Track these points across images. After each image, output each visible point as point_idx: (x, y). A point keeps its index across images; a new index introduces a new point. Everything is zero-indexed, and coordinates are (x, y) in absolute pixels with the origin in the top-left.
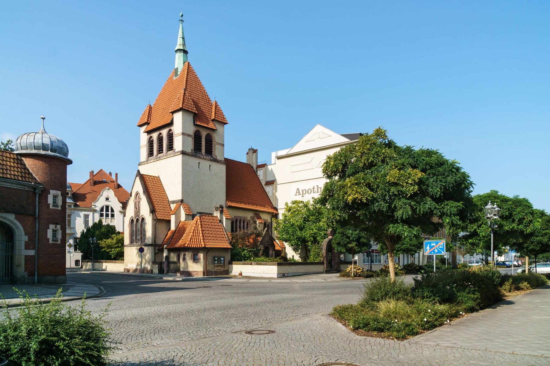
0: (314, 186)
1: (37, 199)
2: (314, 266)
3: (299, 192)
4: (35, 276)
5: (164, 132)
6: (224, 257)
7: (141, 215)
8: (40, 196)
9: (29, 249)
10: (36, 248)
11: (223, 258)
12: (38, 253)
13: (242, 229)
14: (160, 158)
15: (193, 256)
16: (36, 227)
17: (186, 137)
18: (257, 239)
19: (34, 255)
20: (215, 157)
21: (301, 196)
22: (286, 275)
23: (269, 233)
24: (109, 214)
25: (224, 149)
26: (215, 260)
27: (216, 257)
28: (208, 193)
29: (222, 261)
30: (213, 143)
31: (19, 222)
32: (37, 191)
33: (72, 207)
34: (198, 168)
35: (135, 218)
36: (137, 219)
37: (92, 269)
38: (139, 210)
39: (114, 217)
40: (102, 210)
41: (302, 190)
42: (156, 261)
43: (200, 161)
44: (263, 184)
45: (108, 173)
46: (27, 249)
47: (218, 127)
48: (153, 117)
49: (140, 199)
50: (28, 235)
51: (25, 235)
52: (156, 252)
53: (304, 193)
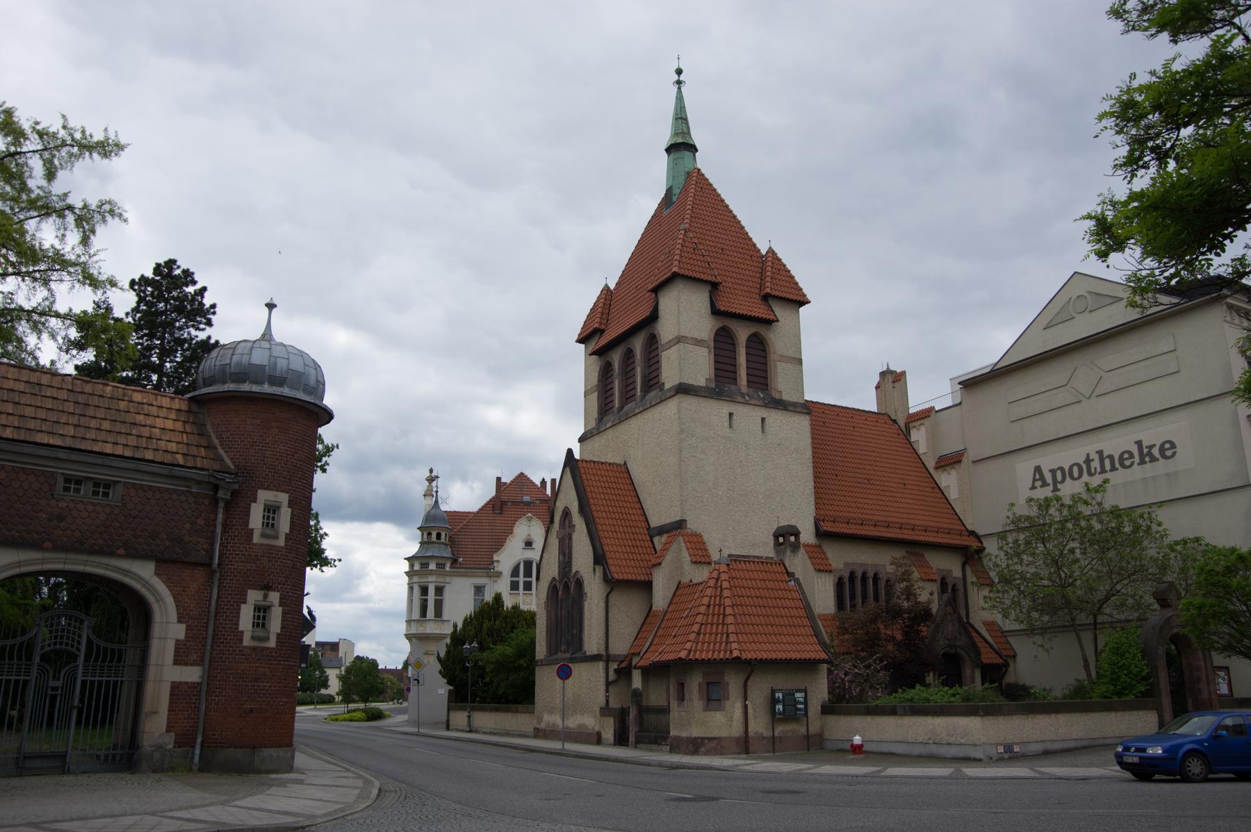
0: (1088, 455)
1: (220, 516)
2: (1119, 714)
3: (1042, 478)
4: (193, 747)
5: (638, 344)
6: (805, 691)
7: (574, 570)
8: (229, 505)
9: (186, 664)
10: (207, 662)
12: (209, 676)
13: (871, 599)
16: (211, 597)
17: (690, 346)
18: (917, 631)
19: (199, 680)
20: (777, 396)
21: (1051, 488)
22: (1016, 749)
23: (955, 611)
26: (778, 701)
27: (779, 691)
28: (761, 497)
29: (801, 703)
30: (772, 357)
31: (164, 582)
32: (221, 494)
33: (448, 568)
34: (727, 430)
35: (561, 581)
36: (566, 582)
38: (570, 557)
40: (515, 572)
41: (1050, 471)
42: (612, 704)
44: (931, 465)
45: (538, 483)
46: (180, 664)
47: (780, 312)
49: (572, 527)
50: (186, 622)
51: (179, 622)
52: (610, 680)
53: (1059, 478)
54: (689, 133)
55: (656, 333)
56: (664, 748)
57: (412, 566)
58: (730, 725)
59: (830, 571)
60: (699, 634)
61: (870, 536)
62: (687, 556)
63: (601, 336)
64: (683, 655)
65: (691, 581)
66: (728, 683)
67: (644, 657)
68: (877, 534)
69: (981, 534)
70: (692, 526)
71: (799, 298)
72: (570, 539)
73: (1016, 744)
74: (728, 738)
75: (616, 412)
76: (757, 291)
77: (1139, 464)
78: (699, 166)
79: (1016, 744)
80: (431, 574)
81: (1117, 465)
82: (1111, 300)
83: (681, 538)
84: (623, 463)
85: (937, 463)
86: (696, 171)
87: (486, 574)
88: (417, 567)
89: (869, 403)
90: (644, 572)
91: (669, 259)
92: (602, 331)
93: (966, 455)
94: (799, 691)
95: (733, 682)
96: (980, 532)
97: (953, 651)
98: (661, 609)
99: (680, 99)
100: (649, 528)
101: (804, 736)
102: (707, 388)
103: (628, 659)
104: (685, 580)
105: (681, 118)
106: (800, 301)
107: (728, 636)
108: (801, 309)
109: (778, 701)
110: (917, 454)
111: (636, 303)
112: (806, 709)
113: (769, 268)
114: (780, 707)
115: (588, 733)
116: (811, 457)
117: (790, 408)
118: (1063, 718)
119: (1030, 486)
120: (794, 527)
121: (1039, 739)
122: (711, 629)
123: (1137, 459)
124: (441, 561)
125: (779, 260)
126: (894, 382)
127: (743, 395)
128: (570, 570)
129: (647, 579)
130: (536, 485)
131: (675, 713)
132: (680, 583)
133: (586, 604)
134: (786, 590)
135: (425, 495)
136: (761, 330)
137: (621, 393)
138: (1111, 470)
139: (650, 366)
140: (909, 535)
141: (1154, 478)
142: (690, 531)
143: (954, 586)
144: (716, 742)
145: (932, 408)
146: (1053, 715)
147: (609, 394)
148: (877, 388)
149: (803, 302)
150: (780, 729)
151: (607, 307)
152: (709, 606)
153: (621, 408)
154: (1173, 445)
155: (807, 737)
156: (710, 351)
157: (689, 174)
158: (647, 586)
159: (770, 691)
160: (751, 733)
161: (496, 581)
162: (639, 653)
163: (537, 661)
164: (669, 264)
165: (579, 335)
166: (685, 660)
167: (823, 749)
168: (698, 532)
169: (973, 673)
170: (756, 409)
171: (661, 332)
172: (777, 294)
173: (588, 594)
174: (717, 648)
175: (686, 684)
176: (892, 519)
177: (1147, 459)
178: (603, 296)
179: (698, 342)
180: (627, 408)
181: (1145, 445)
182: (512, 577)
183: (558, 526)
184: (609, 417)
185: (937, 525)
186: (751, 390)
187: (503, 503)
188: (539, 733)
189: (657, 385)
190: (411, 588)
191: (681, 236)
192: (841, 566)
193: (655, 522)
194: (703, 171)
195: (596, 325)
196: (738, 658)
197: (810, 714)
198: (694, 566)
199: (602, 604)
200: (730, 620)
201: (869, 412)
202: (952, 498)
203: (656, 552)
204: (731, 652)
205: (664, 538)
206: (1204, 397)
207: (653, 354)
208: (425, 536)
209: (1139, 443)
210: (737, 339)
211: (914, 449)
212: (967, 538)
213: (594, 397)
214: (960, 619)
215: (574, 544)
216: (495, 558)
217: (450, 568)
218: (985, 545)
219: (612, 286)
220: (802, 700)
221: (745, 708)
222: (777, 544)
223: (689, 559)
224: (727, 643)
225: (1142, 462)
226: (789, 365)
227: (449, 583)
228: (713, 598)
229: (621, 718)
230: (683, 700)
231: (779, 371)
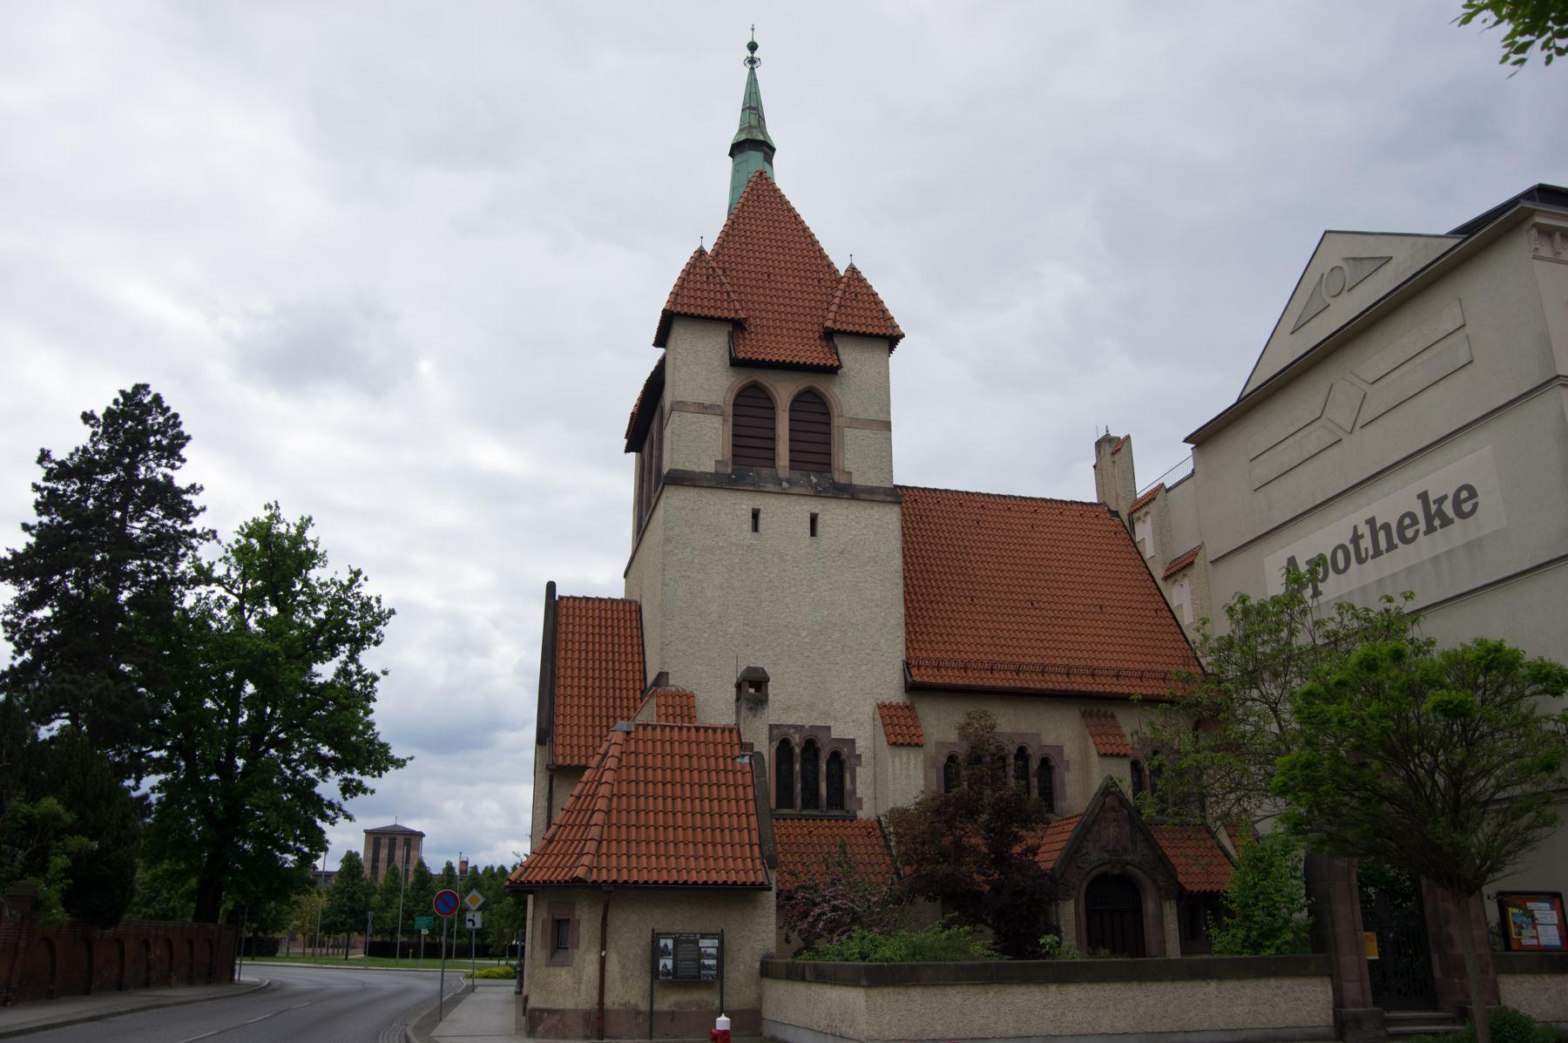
0: (1355, 528)
6: (720, 936)
17: (690, 415)
20: (842, 480)
25: (890, 439)
26: (665, 952)
27: (667, 935)
29: (710, 956)
30: (837, 422)
43: (758, 501)
44: (1159, 574)
47: (852, 357)
58: (578, 991)
64: (580, 872)
66: (579, 921)
74: (574, 1011)
77: (1426, 533)
81: (1396, 540)
82: (1378, 263)
89: (1082, 487)
95: (586, 920)
99: (752, 83)
105: (750, 108)
106: (892, 339)
109: (665, 952)
112: (720, 967)
117: (863, 496)
118: (1075, 992)
121: (1012, 1033)
123: (1422, 526)
126: (1113, 454)
127: (779, 482)
136: (819, 383)
138: (1388, 550)
141: (1449, 553)
142: (674, 689)
144: (557, 1017)
146: (1053, 988)
150: (667, 1001)
154: (1473, 493)
160: (611, 1000)
169: (1160, 908)
170: (802, 500)
177: (1437, 522)
179: (704, 409)
181: (1432, 498)
202: (1186, 623)
206: (1512, 398)
209: (1423, 497)
211: (1139, 553)
220: (713, 951)
221: (603, 962)
225: (1430, 529)
226: (867, 432)
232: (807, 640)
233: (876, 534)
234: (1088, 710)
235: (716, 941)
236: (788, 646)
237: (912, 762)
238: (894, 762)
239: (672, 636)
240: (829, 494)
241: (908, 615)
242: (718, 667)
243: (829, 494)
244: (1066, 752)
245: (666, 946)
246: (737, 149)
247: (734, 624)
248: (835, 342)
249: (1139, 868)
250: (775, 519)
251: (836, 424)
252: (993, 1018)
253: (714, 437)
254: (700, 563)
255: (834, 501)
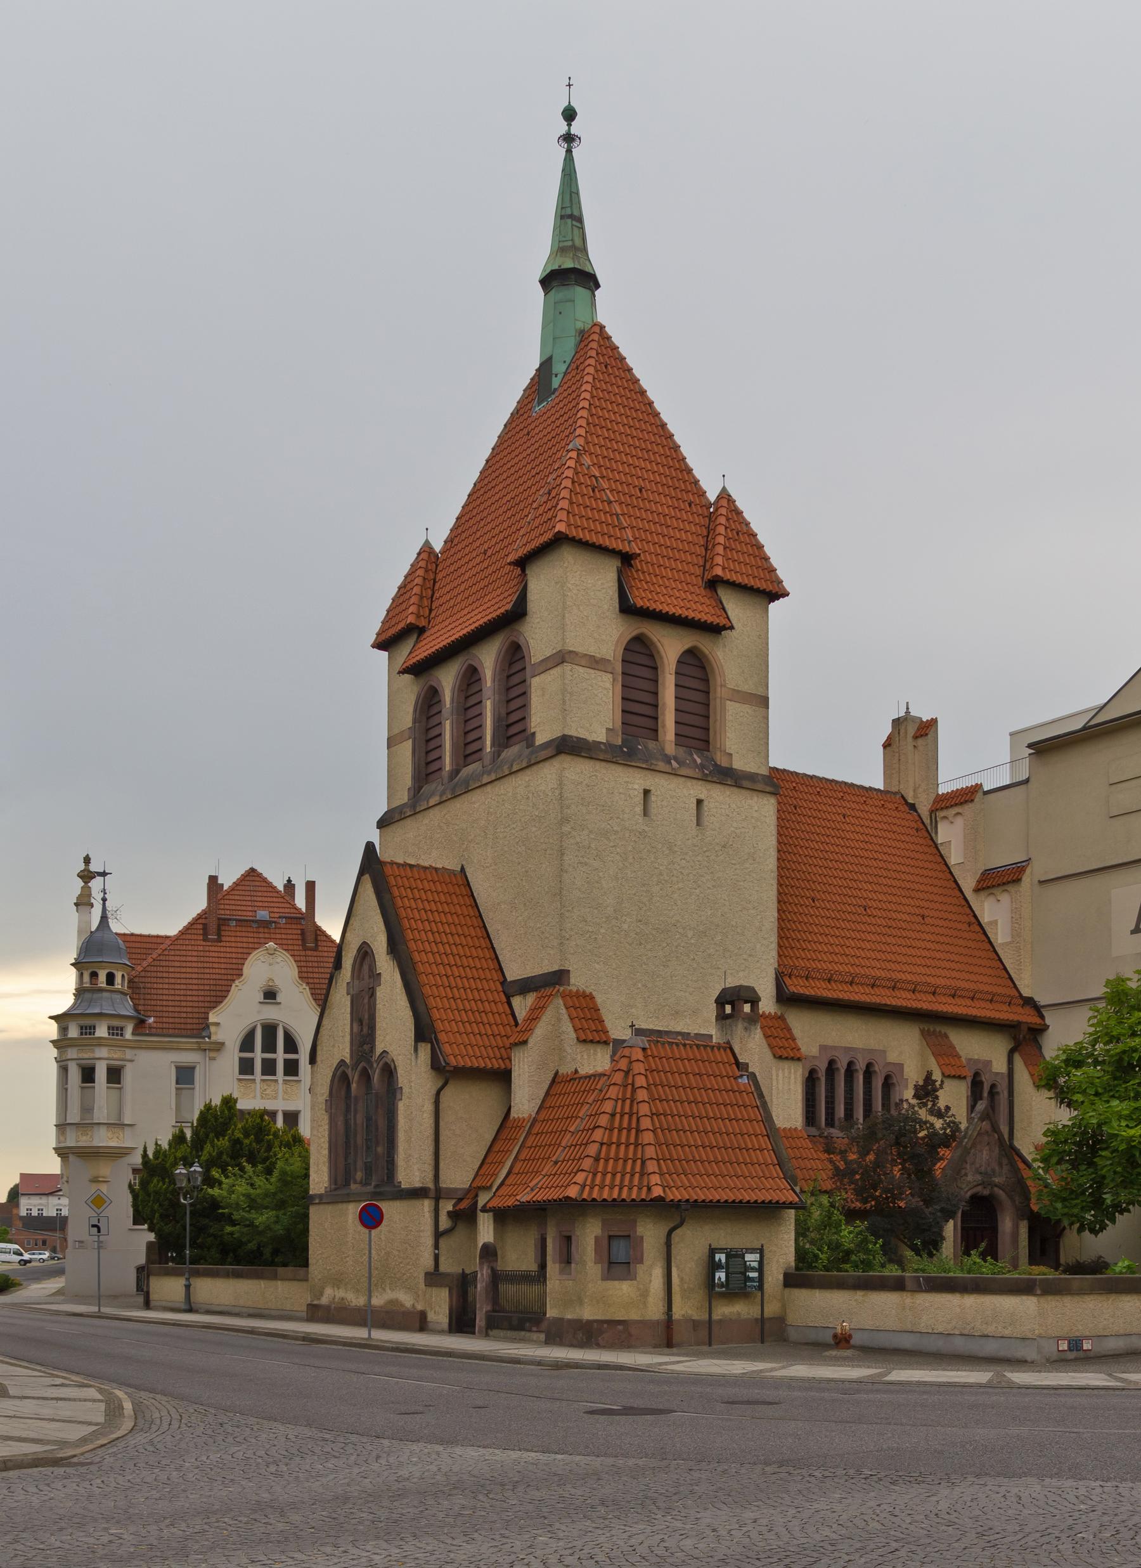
5: (488, 658)
6: (761, 1251)
7: (378, 1051)
11: (757, 1256)
14: (466, 782)
15: (605, 1242)
17: (581, 670)
20: (724, 762)
22: (1087, 1345)
23: (995, 1128)
24: (263, 1051)
28: (690, 934)
29: (753, 1269)
30: (719, 693)
33: (128, 1034)
34: (641, 819)
35: (355, 1066)
37: (187, 1307)
38: (372, 1027)
39: (297, 1075)
40: (247, 1044)
42: (443, 1268)
44: (968, 884)
45: (281, 888)
47: (736, 608)
48: (441, 601)
49: (376, 977)
52: (442, 1228)
54: (584, 250)
55: (522, 642)
56: (535, 1336)
57: (63, 1030)
58: (645, 1303)
59: (799, 1059)
60: (597, 1159)
61: (864, 1003)
62: (571, 1029)
63: (417, 642)
64: (573, 1192)
65: (576, 1071)
66: (642, 1238)
67: (500, 1193)
68: (877, 1000)
69: (1042, 1003)
70: (578, 981)
71: (769, 587)
72: (372, 994)
73: (1087, 1338)
75: (446, 780)
76: (698, 571)
78: (601, 318)
79: (1087, 1338)
80: (100, 1045)
83: (561, 1002)
84: (459, 869)
85: (979, 882)
86: (597, 330)
87: (195, 1046)
88: (73, 1032)
90: (498, 1055)
91: (549, 505)
92: (421, 631)
93: (1028, 871)
94: (752, 1251)
96: (1042, 999)
97: (986, 1192)
98: (526, 1115)
100: (504, 981)
101: (756, 1320)
102: (609, 746)
103: (471, 1195)
104: (566, 1070)
107: (643, 1163)
108: (772, 606)
110: (946, 864)
111: (486, 582)
113: (721, 529)
114: (721, 1275)
115: (404, 1313)
116: (775, 869)
117: (746, 783)
119: (1133, 927)
120: (752, 990)
121: (1122, 1332)
122: (617, 1152)
124: (116, 1023)
125: (739, 513)
126: (916, 737)
128: (372, 1049)
129: (503, 1067)
130: (278, 892)
131: (555, 1280)
132: (557, 1073)
133: (401, 1106)
134: (734, 1092)
135: (76, 904)
137: (454, 745)
139: (508, 701)
140: (924, 1003)
143: (993, 1086)
145: (978, 787)
147: (432, 744)
148: (887, 745)
149: (775, 593)
150: (725, 1310)
151: (429, 584)
152: (613, 1115)
153: (455, 772)
155: (762, 1320)
156: (614, 680)
157: (583, 336)
158: (503, 1077)
159: (707, 1251)
160: (678, 1312)
161: (214, 1059)
162: (491, 1187)
163: (313, 1197)
164: (550, 514)
165: (378, 634)
166: (576, 1200)
167: (785, 1340)
168: (588, 991)
170: (689, 783)
171: (531, 642)
172: (733, 577)
173: (406, 1090)
174: (607, 1182)
175: (573, 1238)
176: (899, 976)
178: (422, 564)
179: (595, 663)
180: (466, 771)
182: (241, 1051)
183: (349, 974)
184: (434, 786)
185: (972, 986)
186: (681, 750)
187: (222, 922)
188: (316, 1313)
189: (523, 735)
190: (63, 1070)
191: (571, 463)
192: (814, 1051)
193: (514, 971)
194: (609, 330)
195: (411, 619)
196: (660, 1199)
197: (766, 1286)
198: (581, 1048)
199: (429, 1107)
200: (648, 1137)
201: (871, 789)
202: (1000, 941)
203: (517, 1024)
204: (649, 1189)
205: (531, 999)
207: (515, 680)
208: (86, 978)
210: (661, 658)
211: (941, 856)
212: (1020, 1010)
213: (406, 749)
214: (1001, 1139)
215: (379, 1006)
216: (212, 1018)
217: (133, 1034)
218: (1048, 1022)
219: (438, 546)
220: (755, 1264)
222: (722, 1017)
223: (573, 1035)
224: (642, 1174)
227: (132, 1061)
228: (620, 1102)
229: (463, 1284)
230: (569, 1262)
231: (729, 717)
232: (693, 941)
233: (754, 828)
234: (932, 1030)
235: (758, 1255)
236: (677, 947)
237: (793, 1077)
238: (777, 1075)
239: (572, 929)
240: (715, 779)
241: (780, 919)
242: (614, 966)
243: (715, 779)
244: (906, 1070)
245: (720, 1260)
246: (549, 281)
247: (628, 920)
248: (719, 592)
249: (1003, 1190)
250: (665, 803)
251: (719, 695)
252: (1112, 1320)
253: (604, 699)
254: (597, 849)
255: (718, 786)
